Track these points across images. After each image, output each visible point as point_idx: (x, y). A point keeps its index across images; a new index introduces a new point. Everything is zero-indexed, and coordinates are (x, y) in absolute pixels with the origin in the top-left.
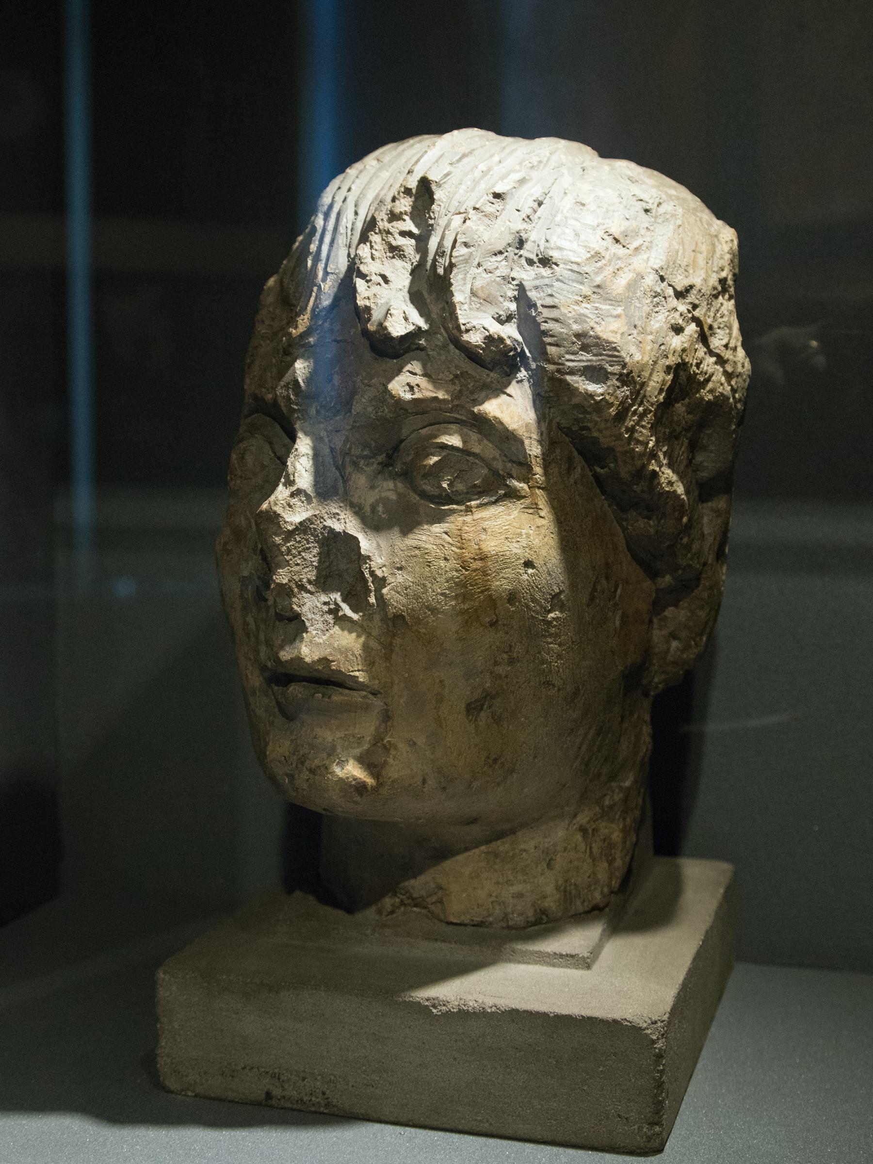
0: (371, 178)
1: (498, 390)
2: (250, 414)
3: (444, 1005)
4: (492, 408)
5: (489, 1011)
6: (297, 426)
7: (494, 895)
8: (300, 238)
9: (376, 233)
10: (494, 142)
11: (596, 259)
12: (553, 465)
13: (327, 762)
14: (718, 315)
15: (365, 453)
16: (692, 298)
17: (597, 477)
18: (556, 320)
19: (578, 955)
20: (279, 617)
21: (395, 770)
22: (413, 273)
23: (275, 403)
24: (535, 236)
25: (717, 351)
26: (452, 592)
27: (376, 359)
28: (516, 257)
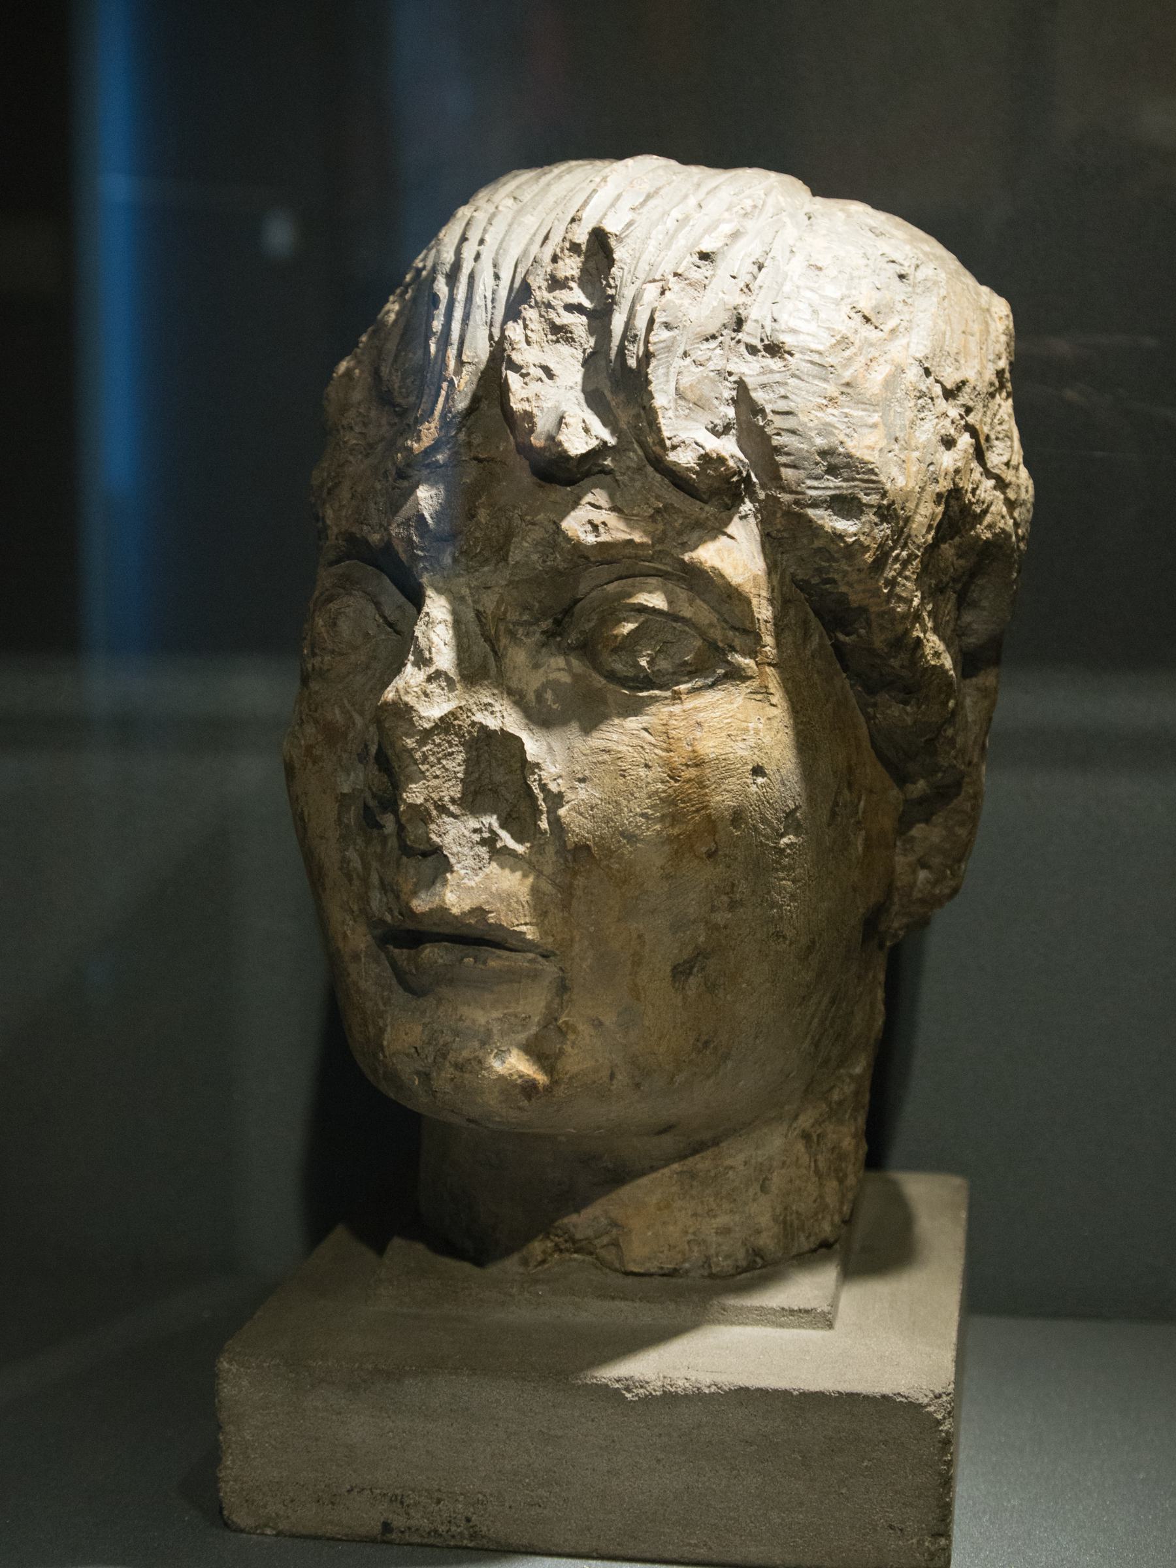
0: (510, 225)
1: (717, 529)
2: (338, 561)
3: (642, 1387)
4: (709, 554)
6: (425, 580)
9: (531, 307)
10: (681, 176)
11: (843, 346)
12: (787, 633)
13: (480, 1054)
14: (996, 421)
15: (525, 618)
16: (964, 398)
17: (838, 648)
18: (793, 432)
21: (574, 1061)
22: (585, 363)
24: (756, 313)
25: (996, 471)
26: (656, 811)
27: (540, 486)
28: (733, 343)
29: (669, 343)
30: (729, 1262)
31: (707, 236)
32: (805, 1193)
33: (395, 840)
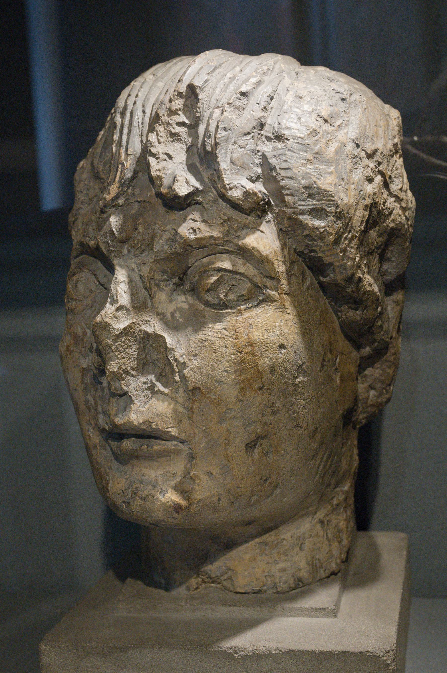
0: (151, 87)
1: (255, 228)
2: (78, 256)
3: (242, 651)
5: (274, 652)
6: (115, 262)
7: (266, 571)
8: (102, 133)
9: (160, 125)
10: (233, 58)
11: (314, 134)
12: (293, 278)
13: (153, 492)
14: (394, 169)
15: (164, 277)
16: (377, 158)
18: (291, 178)
19: (328, 608)
20: (114, 395)
21: (200, 493)
22: (187, 151)
23: (98, 248)
25: (395, 193)
27: (168, 212)
28: (259, 136)
29: (226, 138)
30: (286, 585)
31: (244, 84)
32: (322, 550)
33: (107, 388)
